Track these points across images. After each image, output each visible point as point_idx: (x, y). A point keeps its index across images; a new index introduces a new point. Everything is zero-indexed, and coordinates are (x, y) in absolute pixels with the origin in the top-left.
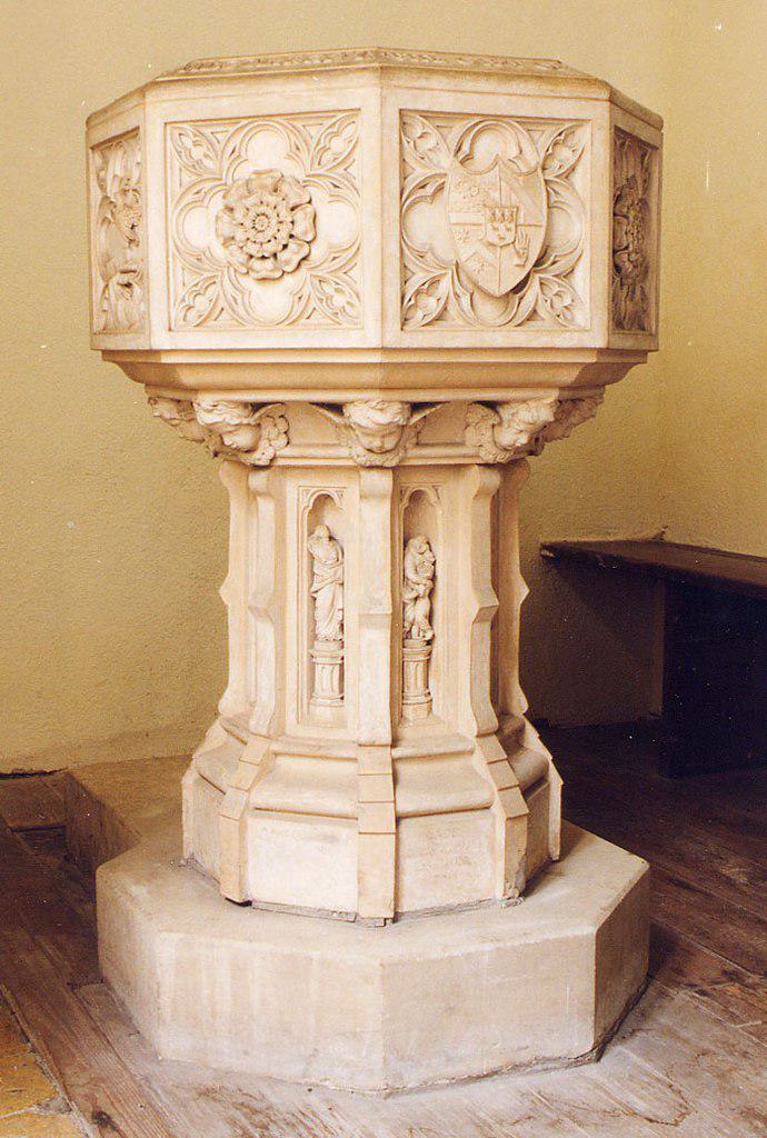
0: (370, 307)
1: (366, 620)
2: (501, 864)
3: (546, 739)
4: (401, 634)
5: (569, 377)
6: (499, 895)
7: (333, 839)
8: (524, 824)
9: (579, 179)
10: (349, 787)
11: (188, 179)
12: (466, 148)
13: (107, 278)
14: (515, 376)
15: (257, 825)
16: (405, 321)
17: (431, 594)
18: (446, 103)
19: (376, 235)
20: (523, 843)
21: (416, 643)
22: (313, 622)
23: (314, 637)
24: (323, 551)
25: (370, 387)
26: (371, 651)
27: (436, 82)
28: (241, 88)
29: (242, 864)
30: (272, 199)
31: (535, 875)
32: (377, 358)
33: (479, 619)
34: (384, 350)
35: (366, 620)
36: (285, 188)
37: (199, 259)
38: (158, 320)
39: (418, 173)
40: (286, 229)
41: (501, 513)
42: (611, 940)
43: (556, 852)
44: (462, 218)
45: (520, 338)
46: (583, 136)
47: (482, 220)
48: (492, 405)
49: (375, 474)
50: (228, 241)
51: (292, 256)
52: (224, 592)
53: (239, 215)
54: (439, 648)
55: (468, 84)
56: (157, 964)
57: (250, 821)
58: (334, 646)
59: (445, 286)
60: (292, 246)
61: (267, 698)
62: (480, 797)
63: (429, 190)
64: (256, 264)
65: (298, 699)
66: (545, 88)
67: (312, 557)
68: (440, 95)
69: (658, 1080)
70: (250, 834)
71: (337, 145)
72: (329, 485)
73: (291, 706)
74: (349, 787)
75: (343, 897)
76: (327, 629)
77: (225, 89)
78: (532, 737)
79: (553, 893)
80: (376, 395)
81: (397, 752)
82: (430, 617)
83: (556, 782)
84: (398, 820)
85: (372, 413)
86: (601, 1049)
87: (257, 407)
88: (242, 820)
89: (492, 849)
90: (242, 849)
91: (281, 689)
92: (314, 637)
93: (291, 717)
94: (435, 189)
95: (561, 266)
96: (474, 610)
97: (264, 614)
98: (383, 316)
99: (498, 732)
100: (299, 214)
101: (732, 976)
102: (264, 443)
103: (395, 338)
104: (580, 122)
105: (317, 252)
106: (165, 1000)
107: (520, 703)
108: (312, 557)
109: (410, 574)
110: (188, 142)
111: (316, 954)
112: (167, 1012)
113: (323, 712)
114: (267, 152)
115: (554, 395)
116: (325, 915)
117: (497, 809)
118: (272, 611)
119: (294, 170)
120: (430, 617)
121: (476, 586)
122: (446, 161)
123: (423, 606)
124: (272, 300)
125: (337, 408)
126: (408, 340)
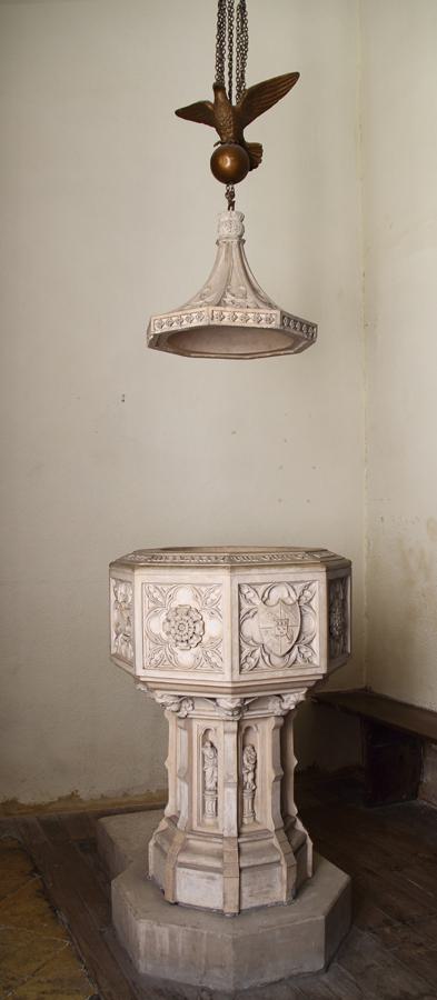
0: (226, 666)
1: (226, 784)
2: (285, 886)
3: (305, 825)
4: (241, 785)
5: (312, 684)
6: (284, 899)
7: (213, 879)
8: (295, 868)
9: (313, 603)
10: (220, 856)
11: (152, 605)
12: (266, 595)
13: (118, 634)
14: (289, 685)
15: (180, 871)
16: (241, 669)
17: (254, 770)
18: (258, 579)
19: (229, 635)
20: (294, 876)
21: (247, 792)
22: (204, 782)
23: (204, 788)
24: (208, 752)
25: (227, 694)
26: (229, 796)
27: (254, 571)
28: (174, 571)
29: (174, 887)
30: (187, 618)
31: (299, 887)
32: (230, 685)
33: (276, 779)
34: (233, 682)
35: (226, 784)
36: (192, 614)
37: (157, 640)
38: (139, 664)
39: (246, 607)
40: (192, 630)
41: (316, 624)
42: (332, 919)
43: (310, 874)
44: (265, 626)
45: (290, 673)
46: (315, 586)
47: (272, 625)
48: (279, 696)
49: (231, 723)
50: (168, 633)
51: (195, 640)
52: (166, 764)
53: (173, 623)
54: (258, 792)
55: (267, 571)
56: (125, 800)
57: (178, 869)
58: (213, 793)
59: (258, 653)
60: (195, 637)
61: (184, 814)
62: (276, 858)
63: (251, 614)
64: (180, 644)
65: (198, 816)
66: (298, 569)
67: (203, 755)
68: (255, 576)
69: (351, 981)
70: (178, 874)
71: (213, 596)
72: (211, 725)
73: (195, 817)
74: (220, 856)
75: (215, 902)
76: (210, 785)
77: (167, 571)
78: (300, 826)
79: (310, 895)
80: (230, 697)
81: (240, 840)
82: (254, 780)
83: (310, 843)
84: (240, 870)
85: (228, 702)
86: (327, 968)
87: (180, 697)
88: (174, 869)
89: (281, 880)
90: (174, 881)
91: (190, 811)
92: (204, 788)
93: (195, 823)
94: (252, 613)
95: (308, 639)
96: (273, 777)
97: (184, 779)
98: (232, 669)
99: (283, 828)
100: (197, 625)
101: (388, 923)
102: (183, 709)
103: (237, 677)
104: (314, 581)
105: (205, 639)
106: (141, 948)
107: (294, 810)
108: (203, 755)
109: (245, 762)
110: (152, 590)
111: (205, 932)
112: (142, 953)
113: (209, 821)
114: (184, 597)
115: (305, 690)
116: (208, 911)
117: (283, 862)
118: (187, 776)
119: (195, 605)
120: (254, 780)
121: (274, 767)
122: (258, 602)
123: (251, 776)
124: (186, 658)
125: (214, 699)
126: (243, 678)
